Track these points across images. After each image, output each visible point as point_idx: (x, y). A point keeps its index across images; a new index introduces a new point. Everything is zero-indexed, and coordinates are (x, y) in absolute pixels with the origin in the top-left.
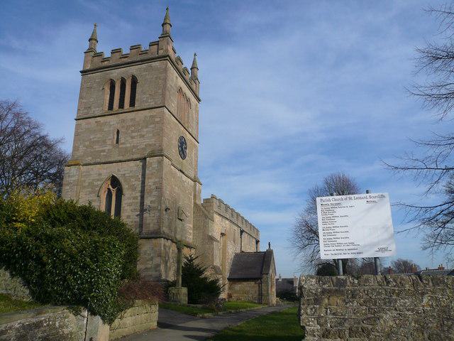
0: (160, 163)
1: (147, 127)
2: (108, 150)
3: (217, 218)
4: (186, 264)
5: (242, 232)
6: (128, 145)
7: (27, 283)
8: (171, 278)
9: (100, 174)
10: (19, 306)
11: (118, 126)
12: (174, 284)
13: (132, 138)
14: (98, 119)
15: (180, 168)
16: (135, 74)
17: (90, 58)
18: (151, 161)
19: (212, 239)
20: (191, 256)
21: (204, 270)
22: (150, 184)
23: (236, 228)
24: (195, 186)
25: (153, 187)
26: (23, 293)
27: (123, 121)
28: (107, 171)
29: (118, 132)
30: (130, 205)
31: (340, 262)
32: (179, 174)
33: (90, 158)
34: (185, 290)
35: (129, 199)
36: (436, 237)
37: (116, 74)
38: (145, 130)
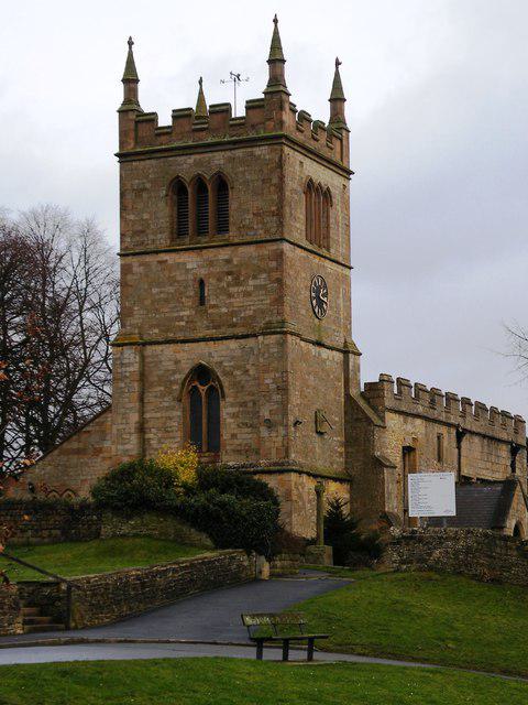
0: (282, 344)
1: (255, 277)
2: (188, 317)
3: (393, 420)
4: (330, 513)
5: (460, 437)
6: (224, 310)
7: (211, 536)
8: (310, 533)
9: (177, 362)
10: (207, 548)
11: (203, 272)
12: (313, 542)
13: (230, 296)
14: (164, 257)
15: (313, 339)
16: (228, 170)
17: (132, 125)
18: (266, 342)
19: (379, 464)
20: (337, 501)
21: (357, 522)
22: (267, 381)
23: (443, 430)
24: (346, 362)
25: (273, 386)
26: (209, 542)
27: (211, 263)
28: (189, 356)
29: (202, 283)
30: (234, 416)
31: (445, 520)
32: (314, 350)
33: (156, 331)
34: (329, 549)
35: (232, 405)
36: (355, 528)
37: (187, 166)
38: (251, 282)
